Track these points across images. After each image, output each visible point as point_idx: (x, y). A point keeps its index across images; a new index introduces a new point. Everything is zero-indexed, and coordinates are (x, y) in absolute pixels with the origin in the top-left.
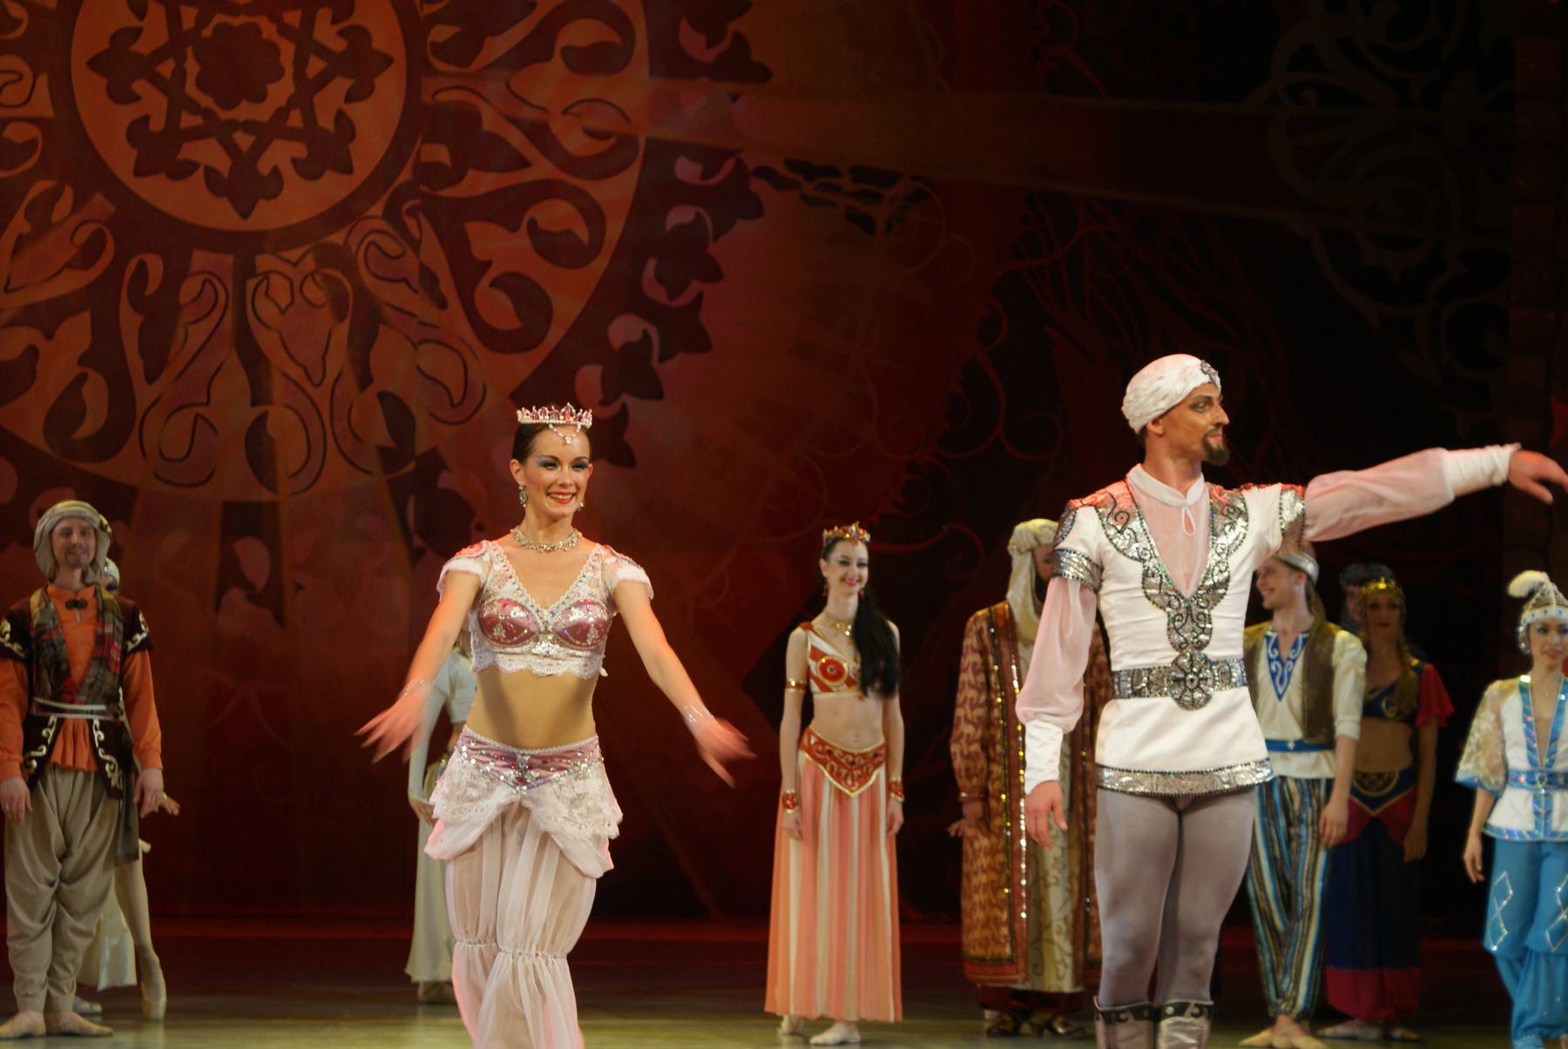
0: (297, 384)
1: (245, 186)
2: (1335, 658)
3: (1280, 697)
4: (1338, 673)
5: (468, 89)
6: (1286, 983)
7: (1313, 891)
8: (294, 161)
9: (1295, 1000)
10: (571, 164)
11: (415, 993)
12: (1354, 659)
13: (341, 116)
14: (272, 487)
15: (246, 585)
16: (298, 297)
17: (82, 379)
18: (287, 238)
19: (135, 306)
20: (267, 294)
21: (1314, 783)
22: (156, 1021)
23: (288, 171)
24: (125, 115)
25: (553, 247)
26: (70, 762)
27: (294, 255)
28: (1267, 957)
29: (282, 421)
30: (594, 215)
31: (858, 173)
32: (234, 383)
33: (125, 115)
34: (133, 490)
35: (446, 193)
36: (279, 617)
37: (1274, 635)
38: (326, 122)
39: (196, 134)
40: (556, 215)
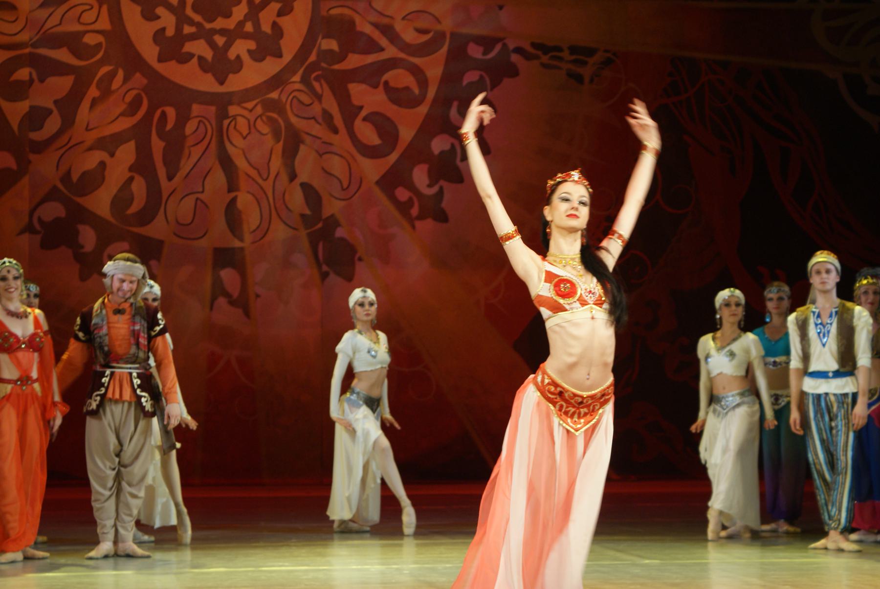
0: (253, 179)
1: (222, 66)
2: (856, 322)
3: (824, 345)
4: (858, 330)
5: (348, 7)
6: (834, 511)
7: (846, 457)
8: (249, 51)
9: (840, 520)
10: (406, 47)
11: (332, 527)
12: (866, 321)
13: (275, 25)
14: (241, 240)
15: (228, 295)
16: (253, 130)
17: (131, 179)
18: (247, 95)
19: (161, 136)
20: (235, 127)
21: (845, 395)
22: (185, 545)
23: (246, 58)
24: (153, 27)
25: (399, 97)
26: (117, 396)
27: (250, 105)
28: (823, 497)
29: (244, 199)
30: (416, 71)
31: (573, 50)
32: (219, 178)
33: (153, 27)
34: (161, 243)
35: (336, 67)
36: (247, 313)
37: (817, 311)
38: (266, 28)
39: (192, 37)
40: (399, 78)
